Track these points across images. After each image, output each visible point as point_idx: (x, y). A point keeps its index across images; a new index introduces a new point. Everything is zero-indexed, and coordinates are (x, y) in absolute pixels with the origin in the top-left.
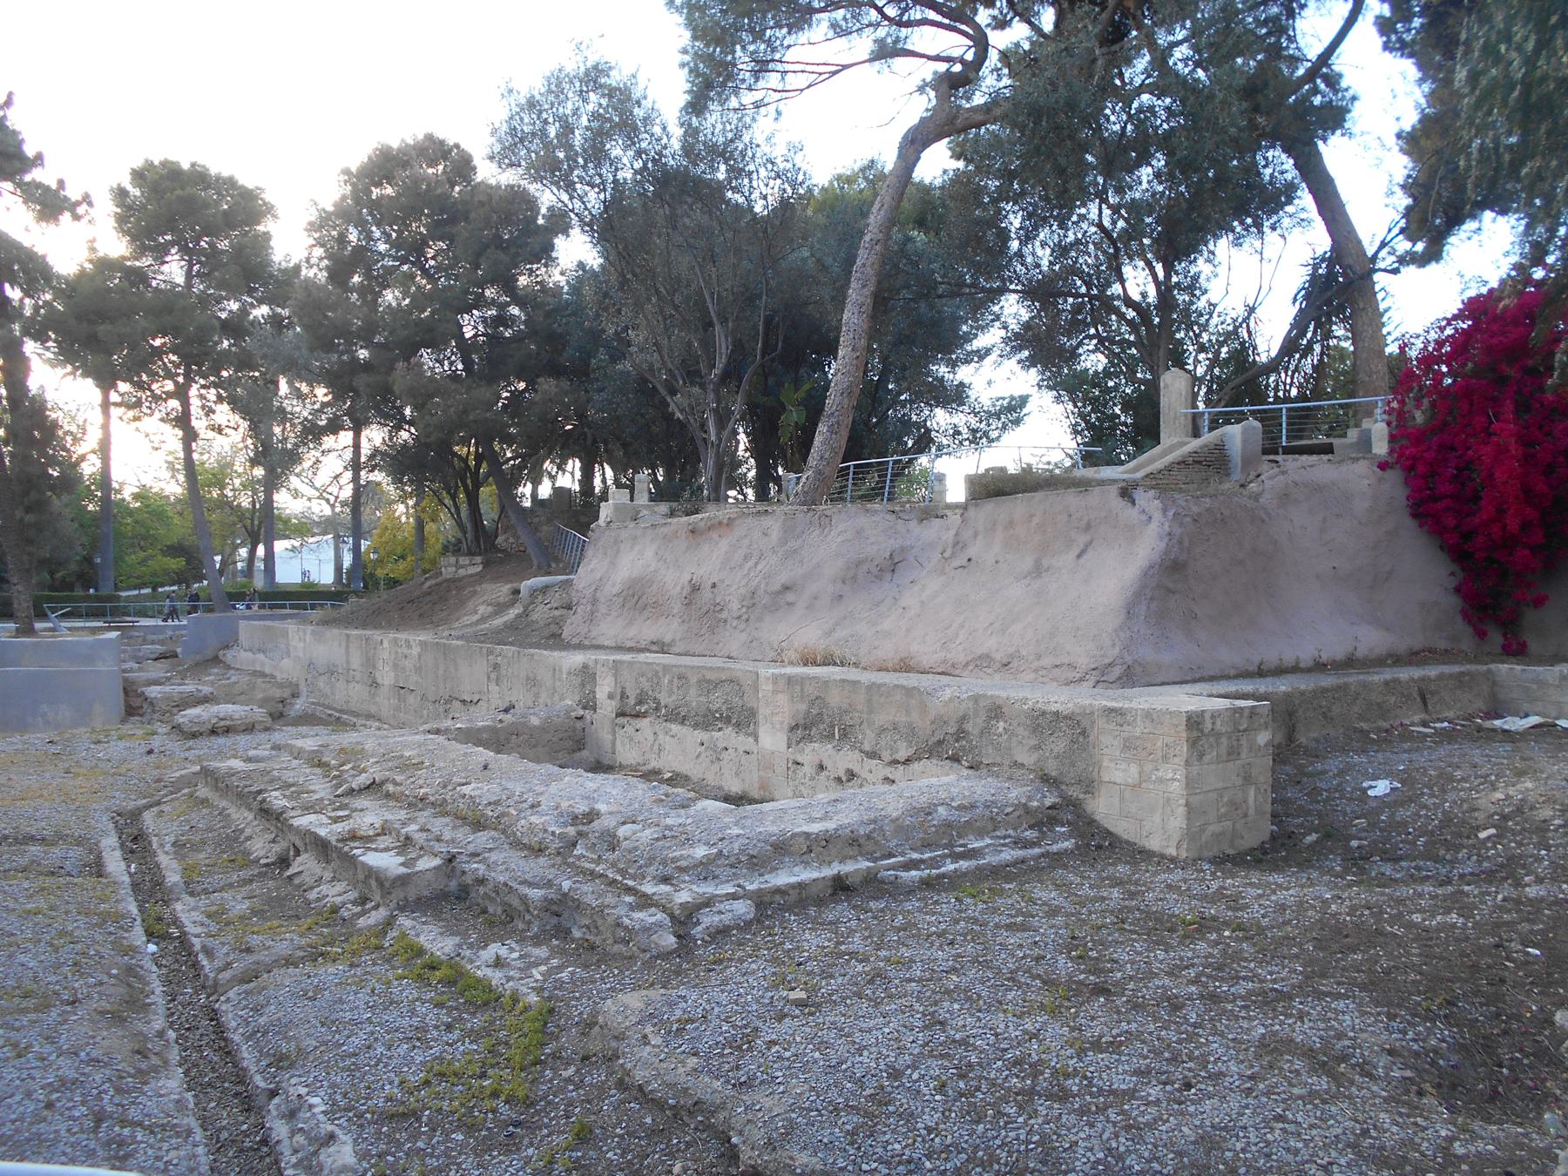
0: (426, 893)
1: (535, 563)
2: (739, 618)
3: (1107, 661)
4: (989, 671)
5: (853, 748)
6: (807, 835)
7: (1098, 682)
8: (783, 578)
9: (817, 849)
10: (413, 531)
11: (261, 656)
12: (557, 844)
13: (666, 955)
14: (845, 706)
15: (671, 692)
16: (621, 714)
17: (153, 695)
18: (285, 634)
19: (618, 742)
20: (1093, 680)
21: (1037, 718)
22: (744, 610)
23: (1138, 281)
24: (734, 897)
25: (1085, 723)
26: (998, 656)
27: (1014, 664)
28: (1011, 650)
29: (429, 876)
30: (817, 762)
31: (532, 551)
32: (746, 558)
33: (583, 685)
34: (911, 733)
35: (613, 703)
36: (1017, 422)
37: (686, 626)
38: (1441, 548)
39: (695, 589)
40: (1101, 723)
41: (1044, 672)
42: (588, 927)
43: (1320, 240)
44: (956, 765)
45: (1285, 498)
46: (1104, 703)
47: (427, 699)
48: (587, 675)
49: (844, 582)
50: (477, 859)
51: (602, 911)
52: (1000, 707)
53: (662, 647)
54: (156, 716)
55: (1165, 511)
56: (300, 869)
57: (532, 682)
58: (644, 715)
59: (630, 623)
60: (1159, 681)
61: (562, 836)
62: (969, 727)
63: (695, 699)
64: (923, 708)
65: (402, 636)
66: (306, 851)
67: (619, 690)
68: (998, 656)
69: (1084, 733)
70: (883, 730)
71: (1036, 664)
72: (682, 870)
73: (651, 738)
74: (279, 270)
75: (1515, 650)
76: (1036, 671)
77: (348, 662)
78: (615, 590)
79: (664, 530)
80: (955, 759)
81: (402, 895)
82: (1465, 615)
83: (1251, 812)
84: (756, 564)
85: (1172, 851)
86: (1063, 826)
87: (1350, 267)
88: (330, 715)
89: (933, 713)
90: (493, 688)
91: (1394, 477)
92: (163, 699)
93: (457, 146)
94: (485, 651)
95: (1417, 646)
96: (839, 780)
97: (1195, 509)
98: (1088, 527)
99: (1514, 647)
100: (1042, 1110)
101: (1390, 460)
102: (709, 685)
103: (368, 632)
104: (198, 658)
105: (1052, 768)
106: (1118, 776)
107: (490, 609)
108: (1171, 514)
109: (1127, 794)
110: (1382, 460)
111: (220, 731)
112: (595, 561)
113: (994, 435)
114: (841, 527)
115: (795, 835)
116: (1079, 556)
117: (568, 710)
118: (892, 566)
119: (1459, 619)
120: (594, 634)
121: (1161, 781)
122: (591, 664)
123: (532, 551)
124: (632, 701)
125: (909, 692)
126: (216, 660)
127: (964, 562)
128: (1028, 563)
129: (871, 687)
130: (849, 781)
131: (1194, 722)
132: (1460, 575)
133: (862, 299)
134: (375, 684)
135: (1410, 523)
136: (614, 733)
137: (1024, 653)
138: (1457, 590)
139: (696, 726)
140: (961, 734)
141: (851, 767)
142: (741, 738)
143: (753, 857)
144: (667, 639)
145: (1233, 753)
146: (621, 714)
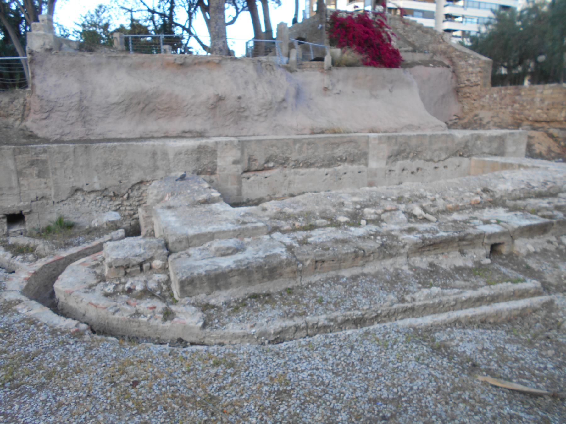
5: (420, 159)
15: (300, 152)
23: (506, 64)
33: (198, 160)
34: (447, 148)
67: (246, 158)
70: (435, 150)
96: (412, 173)
127: (338, 91)
129: (431, 137)
136: (240, 183)
140: (466, 146)
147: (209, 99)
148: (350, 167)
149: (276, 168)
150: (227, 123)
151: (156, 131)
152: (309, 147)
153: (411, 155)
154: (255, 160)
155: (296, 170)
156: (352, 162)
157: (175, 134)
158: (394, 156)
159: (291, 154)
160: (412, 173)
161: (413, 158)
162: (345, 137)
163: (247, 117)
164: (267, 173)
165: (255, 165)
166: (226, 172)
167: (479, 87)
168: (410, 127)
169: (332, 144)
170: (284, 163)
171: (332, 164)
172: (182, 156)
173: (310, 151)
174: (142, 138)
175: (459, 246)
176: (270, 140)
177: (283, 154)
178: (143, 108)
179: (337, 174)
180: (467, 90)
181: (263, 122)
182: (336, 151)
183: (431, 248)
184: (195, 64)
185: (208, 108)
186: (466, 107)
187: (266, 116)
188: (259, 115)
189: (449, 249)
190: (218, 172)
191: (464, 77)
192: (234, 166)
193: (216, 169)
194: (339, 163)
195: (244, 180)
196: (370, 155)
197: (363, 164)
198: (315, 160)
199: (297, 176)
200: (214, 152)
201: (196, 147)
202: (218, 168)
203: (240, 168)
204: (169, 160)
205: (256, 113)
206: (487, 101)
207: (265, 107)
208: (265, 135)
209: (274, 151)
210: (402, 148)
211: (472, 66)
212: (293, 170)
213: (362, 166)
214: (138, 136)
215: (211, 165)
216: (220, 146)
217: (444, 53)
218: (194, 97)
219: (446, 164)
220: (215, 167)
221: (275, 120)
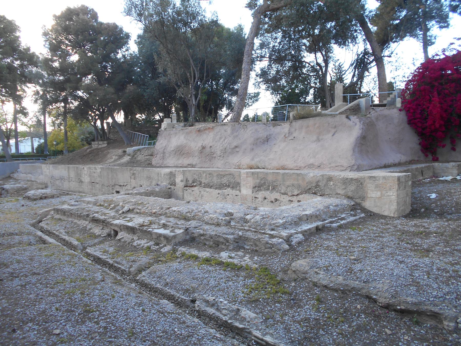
0: (180, 240)
1: (126, 143)
2: (220, 156)
3: (352, 164)
4: (314, 168)
5: (277, 192)
6: (306, 215)
7: (351, 170)
8: (235, 144)
9: (309, 219)
10: (63, 135)
11: (30, 175)
12: (224, 222)
13: (288, 251)
14: (274, 180)
15: (206, 179)
16: (186, 186)
17: (7, 188)
18: (41, 168)
19: (185, 195)
20: (349, 170)
21: (345, 180)
22: (222, 154)
24: (296, 233)
25: (362, 181)
26: (316, 164)
27: (322, 166)
28: (320, 162)
29: (181, 235)
30: (264, 197)
31: (124, 139)
32: (220, 138)
33: (170, 178)
34: (299, 186)
35: (183, 183)
36: (257, 100)
37: (200, 159)
38: (415, 132)
39: (204, 148)
40: (368, 181)
41: (333, 168)
42: (252, 245)
44: (315, 195)
45: (377, 119)
46: (368, 175)
47: (104, 185)
48: (172, 175)
49: (254, 145)
50: (197, 229)
51: (259, 240)
52: (331, 178)
53: (193, 166)
54: (9, 195)
55: (360, 122)
56: (122, 237)
57: (149, 178)
58: (195, 186)
59: (178, 159)
60: (365, 169)
61: (225, 220)
62: (320, 184)
63: (215, 180)
64: (303, 179)
65: (91, 166)
66: (121, 231)
67: (185, 179)
68: (316, 164)
69: (361, 184)
70: (289, 186)
71: (329, 166)
72: (277, 226)
73: (198, 193)
74: (24, 49)
75: (436, 160)
76: (330, 168)
77: (69, 175)
78: (172, 149)
79: (187, 131)
80: (315, 193)
81: (174, 241)
82: (422, 150)
83: (408, 204)
84: (224, 140)
85: (392, 215)
86: (358, 210)
87: (377, 55)
88: (64, 192)
89: (307, 181)
90: (133, 181)
91: (403, 113)
92: (11, 189)
93: (93, 9)
94: (129, 169)
95: (411, 159)
96: (272, 202)
97: (367, 121)
98: (335, 127)
99: (435, 159)
101: (402, 109)
102: (221, 176)
103: (77, 166)
104: (3, 176)
105: (350, 194)
106: (374, 195)
107: (117, 157)
108: (362, 122)
109: (377, 200)
110: (400, 108)
111: (43, 198)
112: (161, 141)
113: (250, 104)
114: (250, 129)
115: (303, 215)
116: (333, 135)
117: (166, 186)
118: (267, 140)
119: (420, 152)
120: (165, 163)
121: (388, 196)
122: (174, 172)
123: (124, 139)
124: (190, 182)
125: (298, 175)
126: (10, 177)
127: (293, 138)
128: (315, 138)
129: (284, 174)
130: (275, 202)
131: (399, 178)
132: (421, 140)
133: (248, 61)
134: (81, 182)
135: (407, 126)
136: (183, 192)
137: (324, 163)
138: (420, 144)
139: (216, 188)
140: (317, 186)
141: (276, 198)
142: (234, 191)
143: (295, 222)
144: (194, 163)
145: (405, 187)
146: (186, 186)
156: (233, 188)
158: (258, 188)
160: (272, 202)
163: (215, 157)
182: (222, 180)
184: (205, 130)
192: (181, 183)
195: (184, 191)
196: (242, 185)
198: (212, 184)
205: (219, 155)
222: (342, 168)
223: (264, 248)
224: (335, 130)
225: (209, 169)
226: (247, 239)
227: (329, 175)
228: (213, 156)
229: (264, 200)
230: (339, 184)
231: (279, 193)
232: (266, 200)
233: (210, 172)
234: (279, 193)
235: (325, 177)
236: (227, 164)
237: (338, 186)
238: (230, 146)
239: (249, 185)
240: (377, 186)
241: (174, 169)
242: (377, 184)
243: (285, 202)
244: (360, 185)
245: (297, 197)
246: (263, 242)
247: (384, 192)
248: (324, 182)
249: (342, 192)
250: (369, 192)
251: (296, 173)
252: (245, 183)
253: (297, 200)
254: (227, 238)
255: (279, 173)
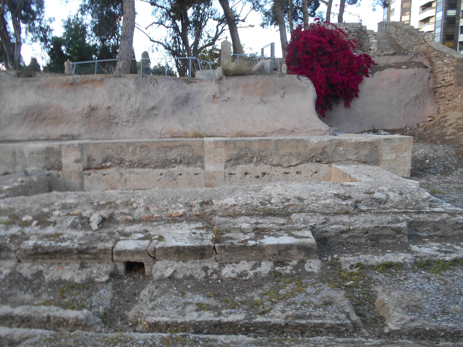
4: (286, 134)
5: (266, 164)
22: (131, 118)
27: (296, 131)
30: (245, 172)
33: (47, 158)
34: (299, 154)
40: (383, 143)
41: (310, 133)
43: (403, 17)
49: (174, 106)
62: (328, 150)
63: (154, 155)
64: (306, 146)
67: (85, 158)
69: (376, 147)
89: (310, 147)
96: (258, 177)
98: (284, 88)
100: (43, 288)
105: (363, 158)
106: (388, 158)
114: (163, 84)
121: (403, 157)
127: (226, 98)
129: (277, 141)
130: (263, 176)
136: (82, 178)
144: (75, 133)
147: (83, 109)
148: (185, 168)
149: (114, 167)
150: (100, 128)
151: (42, 135)
152: (142, 150)
153: (255, 160)
154: (94, 160)
155: (131, 169)
157: (55, 137)
159: (125, 155)
160: (258, 177)
161: (258, 162)
162: (178, 141)
163: (117, 124)
164: (105, 171)
165: (95, 164)
166: (70, 169)
167: (453, 86)
168: (282, 131)
169: (165, 147)
170: (120, 163)
171: (166, 165)
172: (35, 155)
173: (143, 154)
174: (30, 140)
175: (79, 258)
176: (105, 143)
177: (118, 155)
178: (37, 118)
179: (172, 175)
180: (442, 90)
181: (132, 127)
183: (46, 256)
184: (83, 83)
185: (84, 117)
186: (442, 108)
187: (134, 122)
188: (128, 121)
189: (67, 261)
190: (63, 169)
191: (440, 77)
192: (76, 164)
193: (62, 166)
194: (174, 165)
196: (206, 158)
197: (199, 166)
198: (148, 161)
199: (132, 175)
200: (59, 153)
201: (45, 148)
202: (63, 166)
203: (80, 166)
204: (25, 158)
206: (459, 101)
207: (132, 115)
208: (130, 138)
209: (110, 152)
210: (243, 153)
211: (447, 65)
212: (128, 169)
213: (198, 170)
214: (28, 138)
215: (57, 163)
216: (63, 148)
217: (424, 53)
218: (73, 108)
219: (298, 170)
220: (61, 165)
221: (141, 126)
222: (321, 133)
223: (451, 230)
224: (284, 91)
225: (105, 141)
226: (422, 224)
227: (338, 139)
228: (113, 121)
229: (244, 176)
230: (351, 149)
231: (268, 165)
232: (248, 176)
233: (142, 144)
234: (268, 165)
235: (334, 142)
236: (143, 132)
237: (349, 150)
238: (143, 107)
239: (220, 157)
240: (392, 148)
241: (56, 144)
242: (393, 147)
243: (278, 175)
244: (375, 149)
245: (296, 168)
246: (450, 223)
247: (399, 154)
248: (333, 148)
249: (353, 157)
250: (384, 154)
251: (296, 139)
252: (211, 156)
253: (296, 171)
254: (399, 227)
255: (270, 140)
